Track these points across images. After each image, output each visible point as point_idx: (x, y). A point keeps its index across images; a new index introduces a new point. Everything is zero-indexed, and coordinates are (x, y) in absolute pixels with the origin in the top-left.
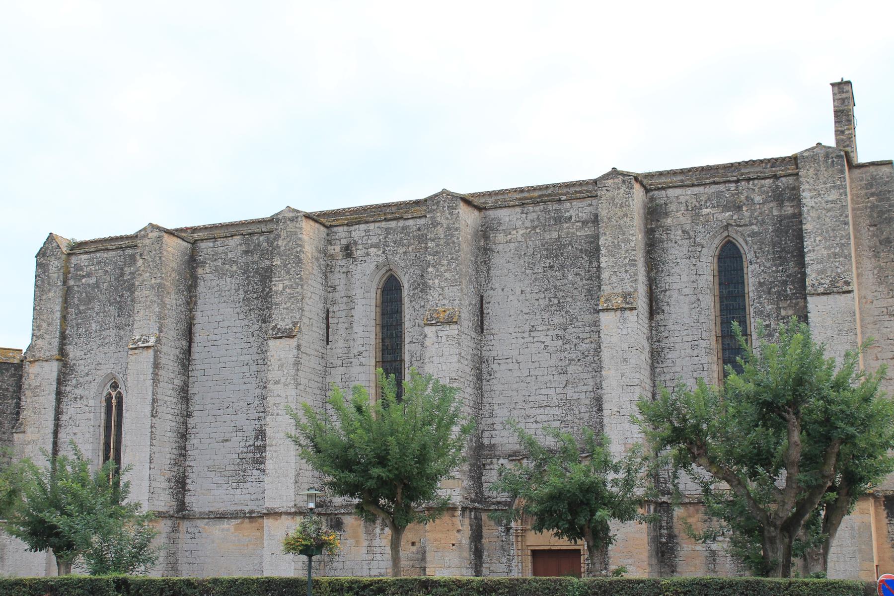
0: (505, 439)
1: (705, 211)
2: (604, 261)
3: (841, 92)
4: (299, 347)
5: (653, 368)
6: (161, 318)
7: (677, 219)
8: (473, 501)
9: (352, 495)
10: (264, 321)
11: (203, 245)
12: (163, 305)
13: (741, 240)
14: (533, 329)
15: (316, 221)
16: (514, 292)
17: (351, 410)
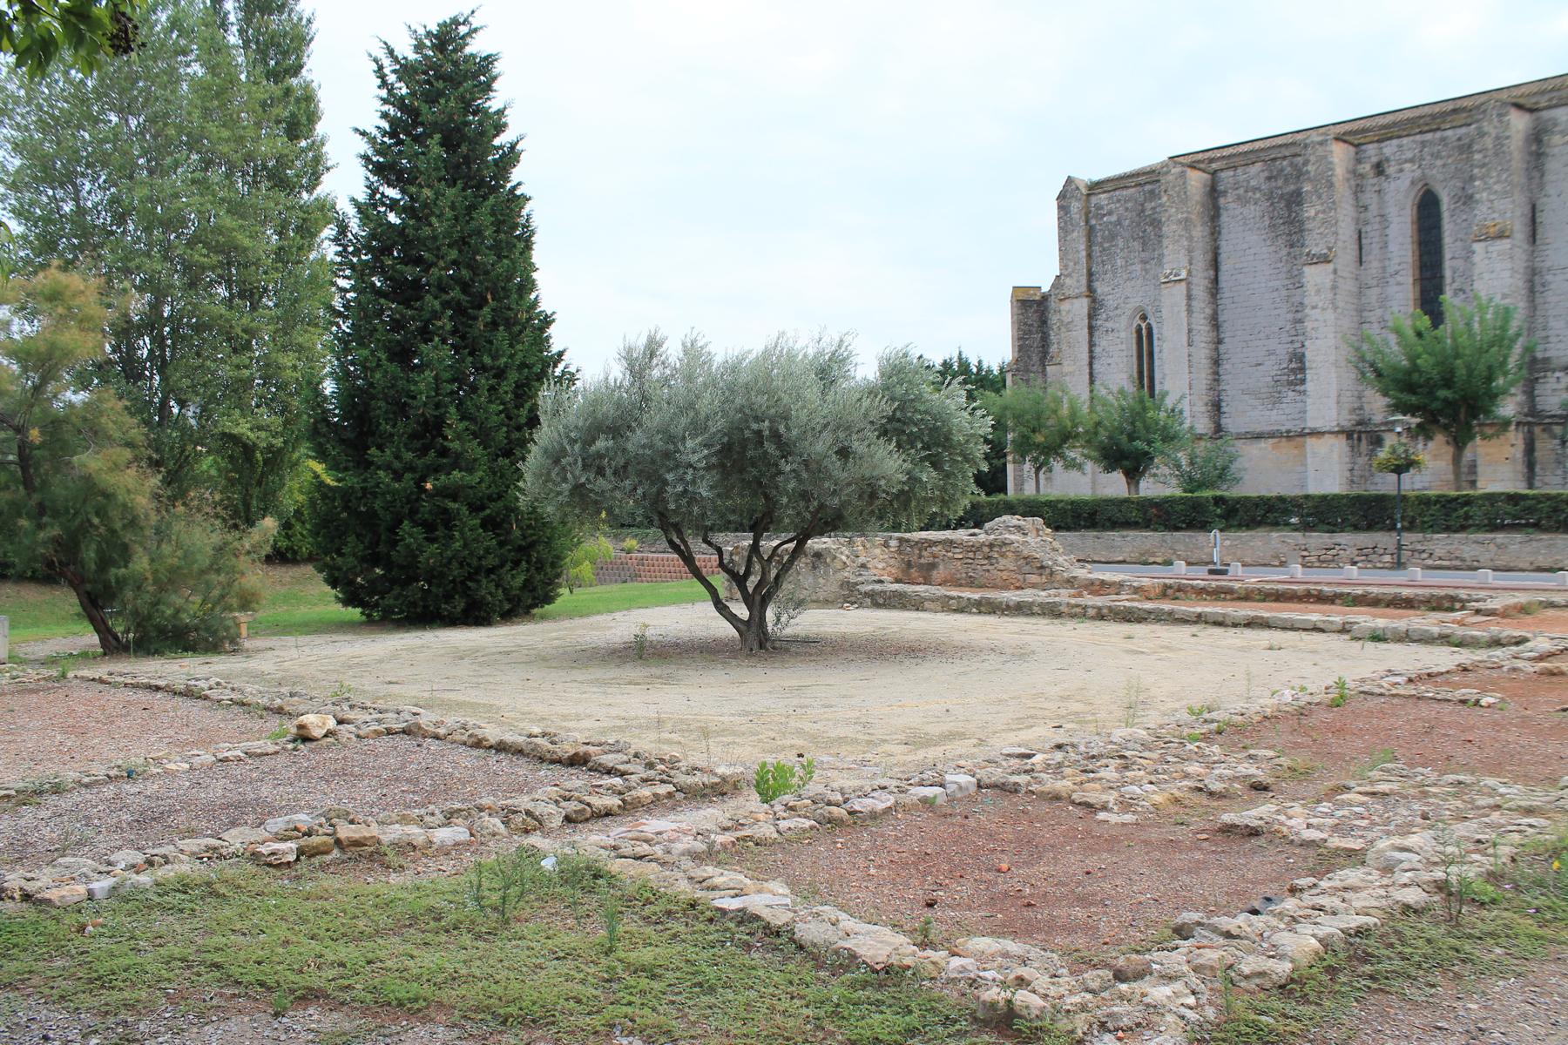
4: (1335, 272)
8: (1526, 415)
9: (1413, 415)
10: (1292, 246)
11: (1223, 175)
12: (1190, 239)
17: (1410, 333)
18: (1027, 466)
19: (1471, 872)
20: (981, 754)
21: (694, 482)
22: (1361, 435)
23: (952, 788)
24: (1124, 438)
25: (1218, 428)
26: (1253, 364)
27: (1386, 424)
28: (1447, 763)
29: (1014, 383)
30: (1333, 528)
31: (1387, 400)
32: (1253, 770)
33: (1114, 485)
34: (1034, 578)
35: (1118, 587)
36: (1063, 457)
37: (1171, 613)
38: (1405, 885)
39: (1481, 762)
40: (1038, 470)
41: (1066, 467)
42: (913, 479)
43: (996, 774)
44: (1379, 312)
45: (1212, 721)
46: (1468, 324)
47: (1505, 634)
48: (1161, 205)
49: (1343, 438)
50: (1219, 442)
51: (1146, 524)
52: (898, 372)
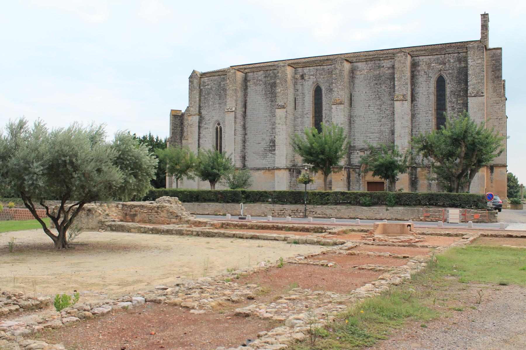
0: (359, 143)
1: (433, 65)
2: (396, 83)
3: (484, 18)
4: (286, 112)
5: (412, 120)
6: (236, 101)
7: (422, 67)
9: (311, 164)
10: (272, 102)
11: (249, 74)
12: (237, 96)
13: (445, 75)
14: (369, 106)
15: (291, 66)
16: (363, 92)
17: (311, 135)
18: (174, 177)
19: (319, 326)
20: (149, 288)
21: (36, 180)
22: (294, 170)
23: (135, 302)
24: (210, 168)
25: (244, 166)
26: (256, 145)
27: (302, 166)
28: (316, 287)
29: (170, 146)
30: (283, 203)
31: (303, 158)
32: (248, 292)
33: (206, 186)
34: (174, 220)
35: (205, 224)
36: (187, 174)
37: (224, 234)
38: (297, 332)
39: (326, 286)
40: (177, 179)
41: (188, 178)
42: (126, 182)
43: (153, 296)
44: (301, 127)
45: (235, 274)
46: (330, 133)
47: (338, 241)
48: (227, 83)
49: (287, 171)
50: (244, 171)
51: (217, 200)
52: (124, 141)
